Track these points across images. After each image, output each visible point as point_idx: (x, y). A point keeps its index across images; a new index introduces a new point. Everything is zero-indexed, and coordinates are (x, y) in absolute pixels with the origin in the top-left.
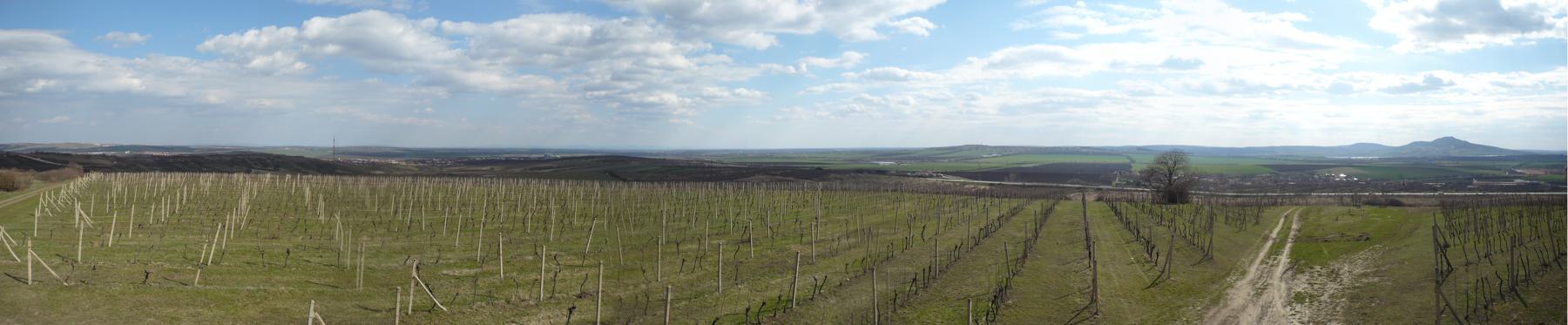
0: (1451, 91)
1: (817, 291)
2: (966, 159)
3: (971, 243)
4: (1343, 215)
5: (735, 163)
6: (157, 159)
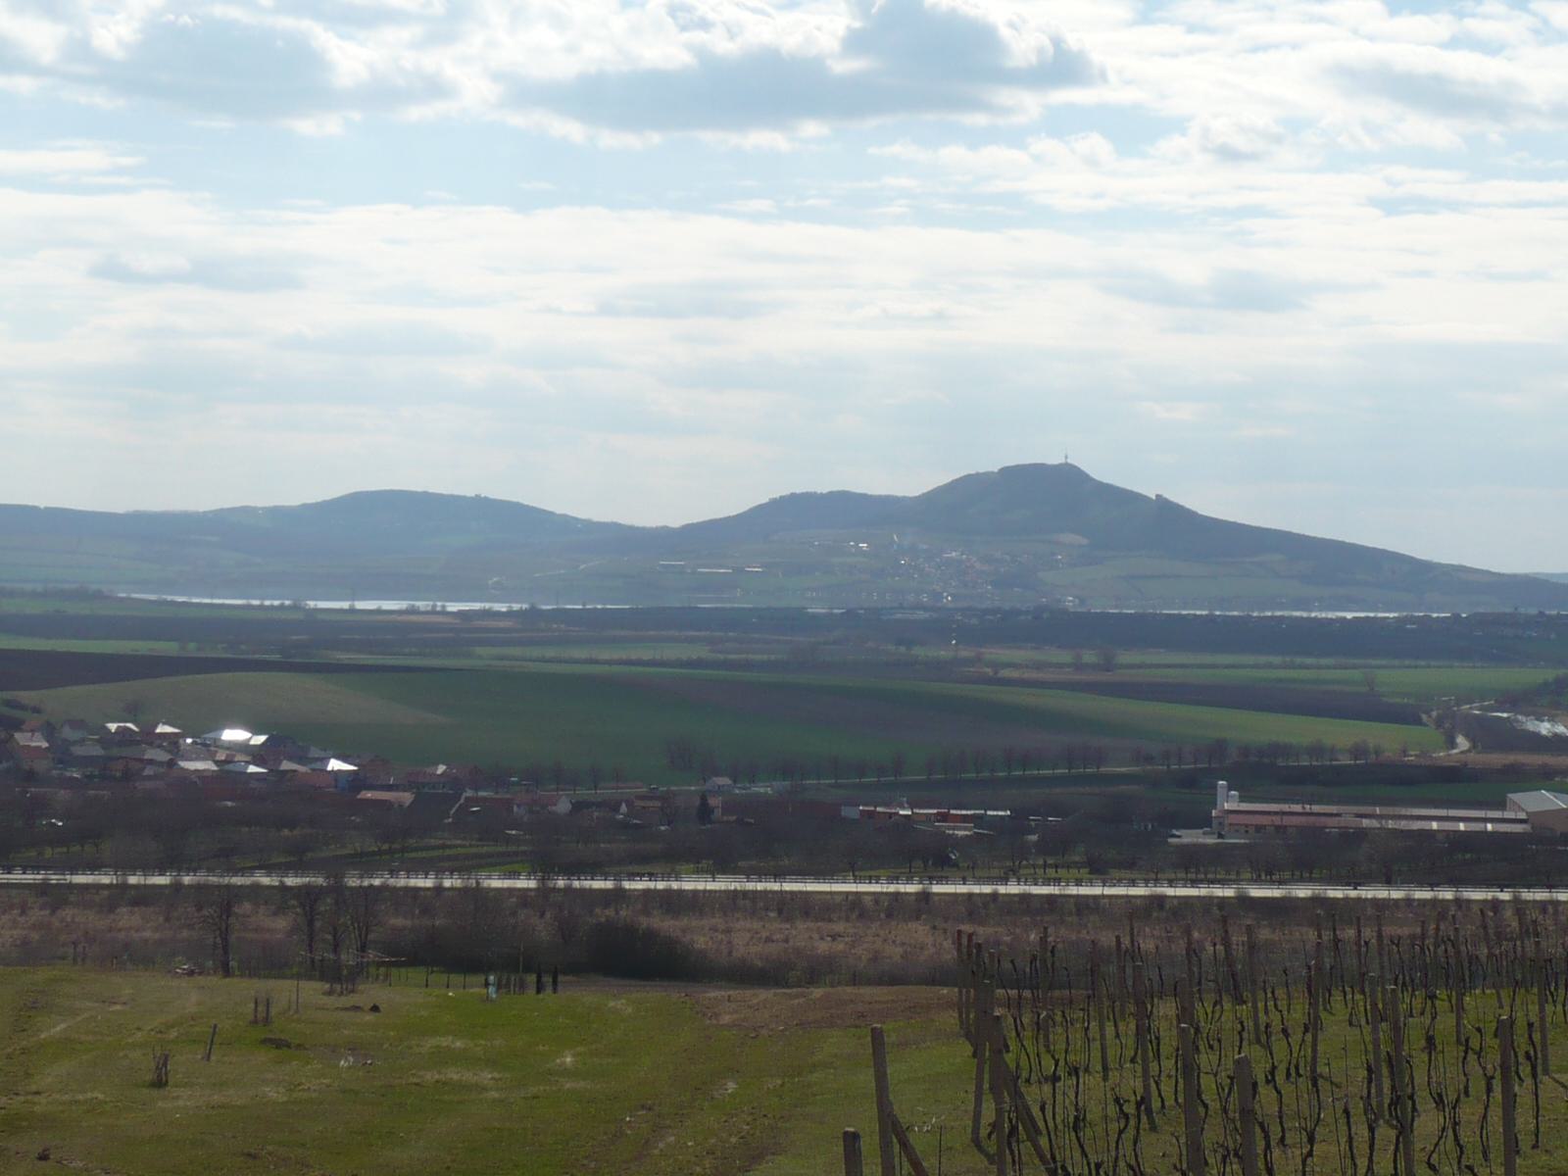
0: (1061, 124)
4: (212, 1040)
6: (1175, 902)
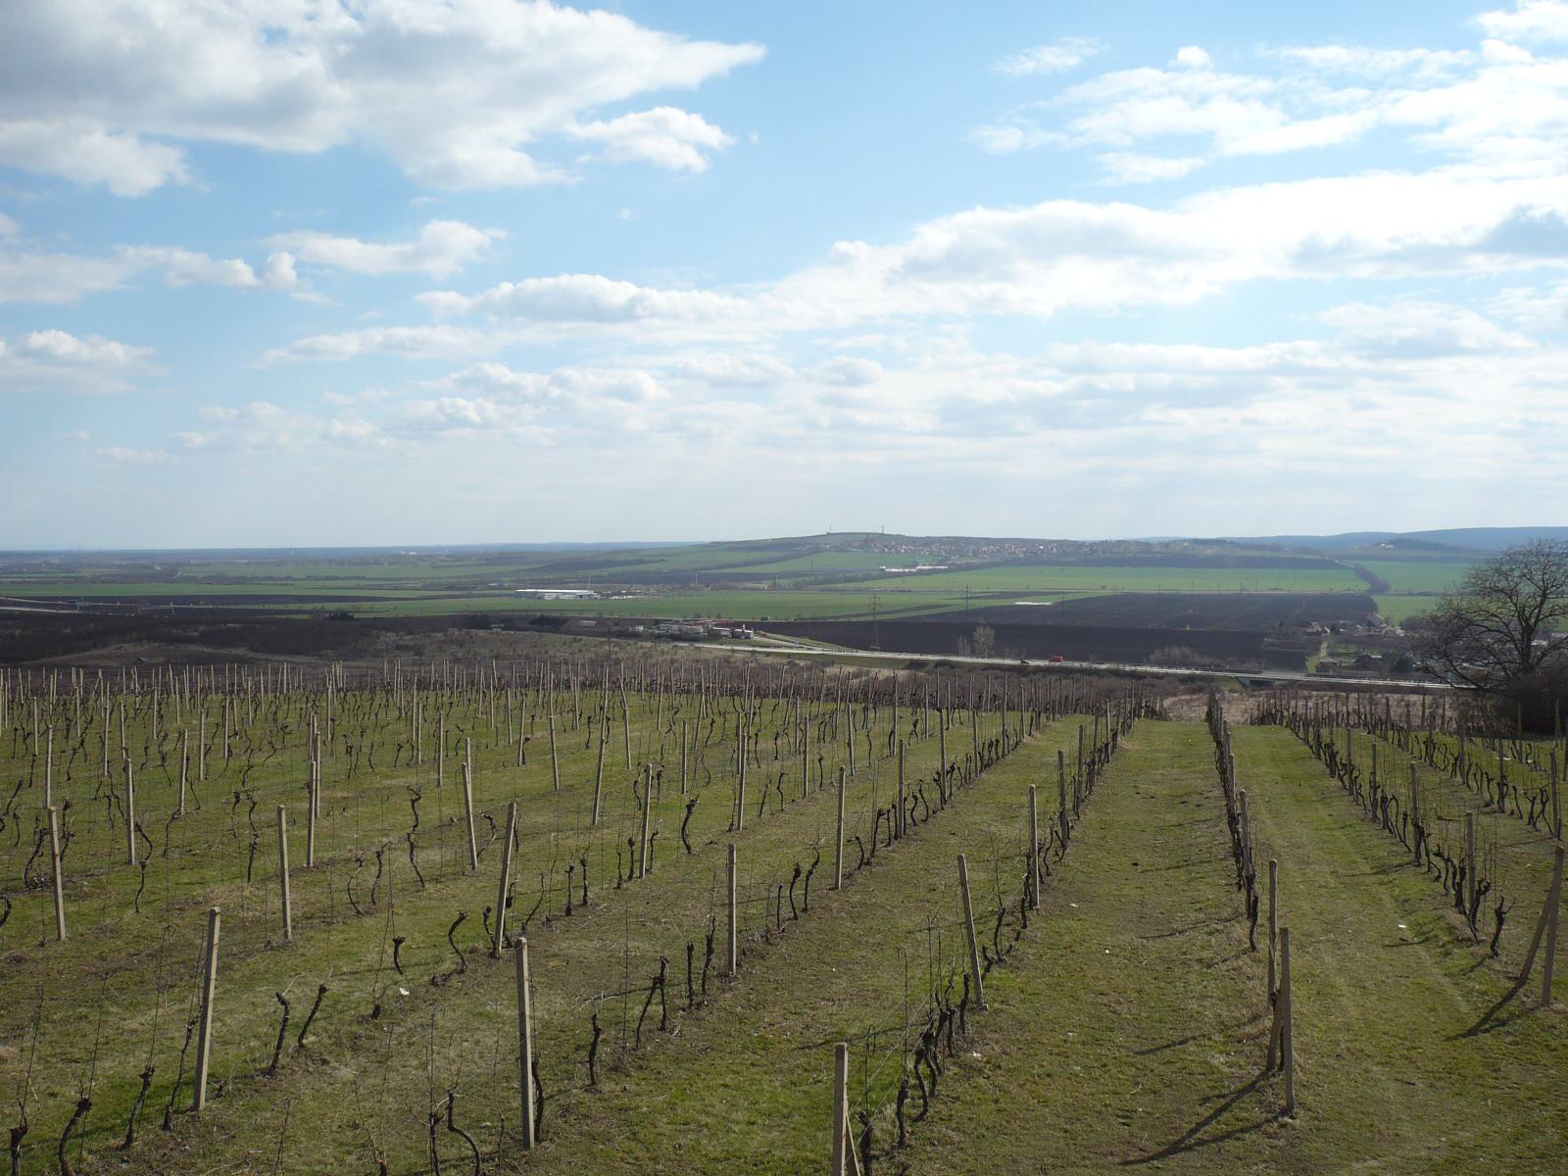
1: (291, 1042)
2: (827, 580)
3: (848, 857)
5: (36, 601)
